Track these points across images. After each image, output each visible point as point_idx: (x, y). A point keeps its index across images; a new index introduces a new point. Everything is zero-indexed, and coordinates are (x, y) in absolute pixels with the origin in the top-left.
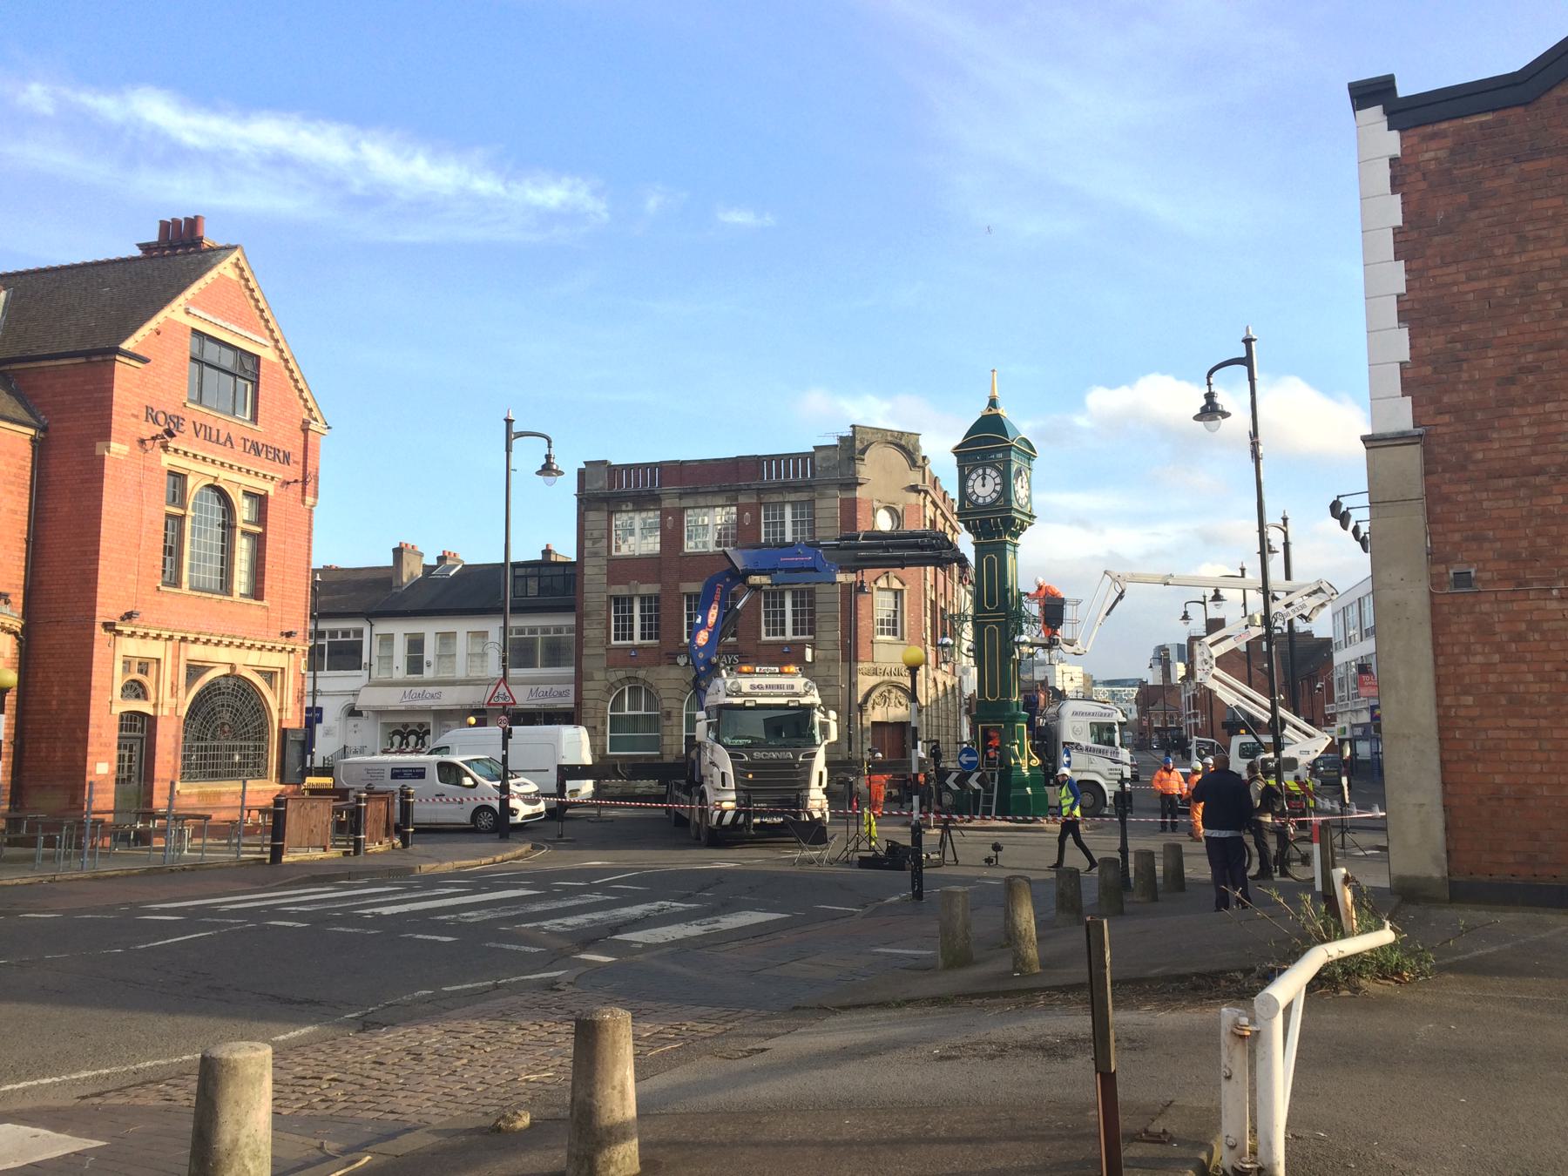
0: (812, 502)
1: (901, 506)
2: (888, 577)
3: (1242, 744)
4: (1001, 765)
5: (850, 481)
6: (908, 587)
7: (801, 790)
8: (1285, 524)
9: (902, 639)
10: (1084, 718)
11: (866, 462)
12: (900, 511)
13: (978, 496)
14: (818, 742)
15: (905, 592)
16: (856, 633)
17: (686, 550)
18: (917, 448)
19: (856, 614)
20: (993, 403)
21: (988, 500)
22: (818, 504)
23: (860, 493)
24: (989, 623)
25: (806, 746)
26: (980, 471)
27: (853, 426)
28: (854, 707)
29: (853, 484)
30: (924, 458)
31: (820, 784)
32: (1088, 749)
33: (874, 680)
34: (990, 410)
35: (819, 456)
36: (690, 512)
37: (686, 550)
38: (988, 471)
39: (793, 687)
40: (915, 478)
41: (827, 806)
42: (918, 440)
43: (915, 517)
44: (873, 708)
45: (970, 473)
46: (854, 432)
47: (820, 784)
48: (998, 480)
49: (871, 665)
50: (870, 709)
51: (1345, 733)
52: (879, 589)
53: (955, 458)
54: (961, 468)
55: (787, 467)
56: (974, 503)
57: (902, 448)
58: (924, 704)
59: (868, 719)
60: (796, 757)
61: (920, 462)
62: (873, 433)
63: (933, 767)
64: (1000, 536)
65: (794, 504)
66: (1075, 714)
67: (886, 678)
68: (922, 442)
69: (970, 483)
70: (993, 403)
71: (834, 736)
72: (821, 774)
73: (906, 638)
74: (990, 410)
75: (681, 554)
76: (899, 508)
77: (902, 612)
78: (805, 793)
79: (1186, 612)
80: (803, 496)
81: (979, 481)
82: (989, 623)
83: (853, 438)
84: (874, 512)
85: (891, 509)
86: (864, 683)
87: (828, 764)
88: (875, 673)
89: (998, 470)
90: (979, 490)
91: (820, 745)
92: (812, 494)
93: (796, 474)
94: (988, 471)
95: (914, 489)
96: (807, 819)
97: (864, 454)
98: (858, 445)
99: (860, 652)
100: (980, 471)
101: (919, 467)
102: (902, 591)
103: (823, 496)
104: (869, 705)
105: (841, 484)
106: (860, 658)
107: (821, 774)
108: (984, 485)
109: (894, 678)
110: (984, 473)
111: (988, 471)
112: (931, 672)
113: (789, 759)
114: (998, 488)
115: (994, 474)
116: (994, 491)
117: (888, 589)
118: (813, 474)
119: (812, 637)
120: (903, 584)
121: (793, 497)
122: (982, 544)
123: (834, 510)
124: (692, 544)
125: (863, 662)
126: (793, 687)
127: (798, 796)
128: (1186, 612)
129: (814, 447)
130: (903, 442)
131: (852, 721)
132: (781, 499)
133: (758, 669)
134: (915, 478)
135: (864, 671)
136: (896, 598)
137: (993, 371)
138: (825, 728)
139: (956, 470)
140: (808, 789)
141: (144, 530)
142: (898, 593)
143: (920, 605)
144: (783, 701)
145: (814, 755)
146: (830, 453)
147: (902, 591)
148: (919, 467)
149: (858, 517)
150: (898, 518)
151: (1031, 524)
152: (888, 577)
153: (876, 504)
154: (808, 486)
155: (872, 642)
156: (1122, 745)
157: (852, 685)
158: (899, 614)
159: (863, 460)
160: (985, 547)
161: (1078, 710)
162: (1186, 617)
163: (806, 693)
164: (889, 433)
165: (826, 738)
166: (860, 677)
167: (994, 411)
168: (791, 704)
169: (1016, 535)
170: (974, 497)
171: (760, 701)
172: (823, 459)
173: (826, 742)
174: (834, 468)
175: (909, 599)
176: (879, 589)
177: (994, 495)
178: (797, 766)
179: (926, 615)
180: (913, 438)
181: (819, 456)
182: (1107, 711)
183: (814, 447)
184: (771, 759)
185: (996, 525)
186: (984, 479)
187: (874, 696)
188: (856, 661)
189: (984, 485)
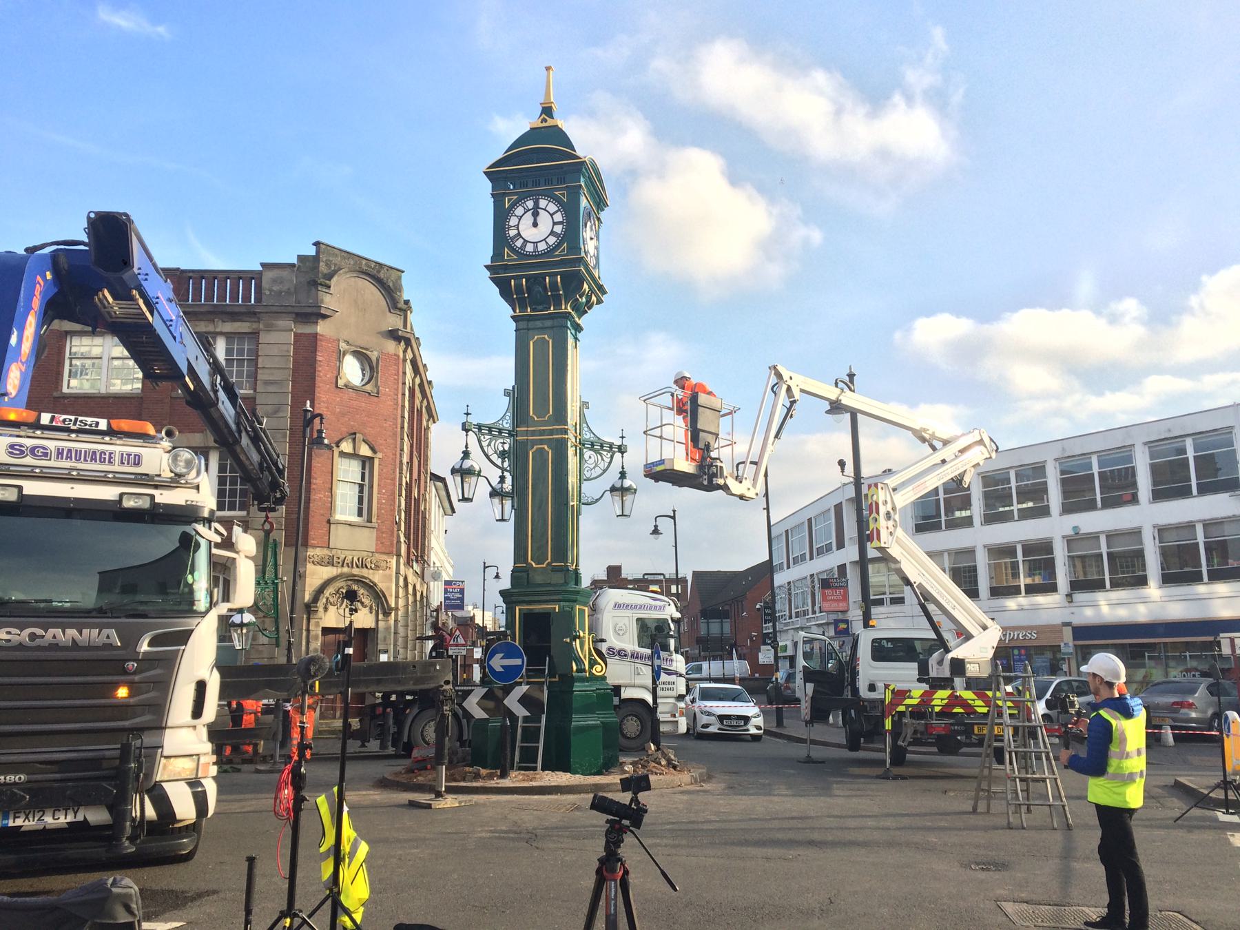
0: (254, 335)
1: (376, 353)
2: (354, 440)
3: (874, 641)
4: (551, 675)
5: (309, 310)
6: (379, 455)
7: (139, 731)
8: (852, 381)
9: (369, 521)
10: (628, 613)
11: (332, 290)
12: (374, 359)
13: (526, 241)
14: (202, 602)
15: (376, 462)
16: (307, 508)
17: (65, 390)
18: (399, 288)
19: (309, 483)
20: (547, 111)
21: (542, 247)
22: (264, 338)
23: (322, 328)
24: (534, 443)
25: (163, 614)
26: (530, 204)
27: (317, 244)
28: (299, 606)
29: (315, 315)
30: (407, 302)
31: (197, 712)
32: (634, 656)
33: (327, 572)
34: (544, 120)
35: (268, 276)
36: (76, 341)
37: (65, 390)
38: (543, 203)
39: (137, 460)
40: (394, 321)
41: (214, 770)
42: (400, 278)
43: (392, 370)
44: (326, 609)
45: (513, 206)
46: (318, 252)
47: (197, 712)
48: (558, 217)
49: (326, 552)
50: (321, 609)
51: (786, 651)
52: (343, 455)
53: (489, 184)
54: (498, 198)
55: (223, 289)
56: (520, 253)
57: (380, 283)
58: (393, 605)
59: (317, 624)
60: (130, 641)
61: (401, 305)
62: (344, 258)
63: (450, 677)
64: (558, 305)
65: (229, 337)
66: (618, 606)
67: (346, 570)
68: (405, 281)
69: (513, 221)
70: (547, 111)
71: (245, 590)
72: (201, 687)
73: (374, 520)
74: (544, 120)
75: (55, 394)
76: (374, 356)
77: (371, 487)
78: (148, 739)
79: (656, 526)
80: (243, 327)
81: (528, 219)
82: (534, 443)
83: (316, 258)
84: (340, 356)
85: (361, 355)
86: (316, 575)
87: (227, 666)
88: (331, 562)
89: (557, 200)
90: (528, 232)
91: (203, 614)
92: (255, 326)
93: (234, 297)
94: (543, 203)
95: (394, 335)
96: (150, 812)
97: (330, 279)
98: (323, 267)
99: (311, 533)
100: (530, 204)
101: (400, 309)
102: (371, 459)
103: (270, 328)
104: (321, 604)
105: (297, 314)
106: (312, 542)
107: (201, 687)
108: (535, 225)
109: (356, 571)
110: (536, 206)
111: (543, 203)
112: (402, 567)
113: (109, 647)
114: (558, 229)
115: (552, 208)
116: (552, 233)
117: (354, 456)
118: (258, 299)
119: (244, 513)
120: (374, 451)
121: (228, 327)
122: (529, 318)
123: (285, 347)
124: (74, 383)
125: (315, 547)
126: (137, 460)
127: (125, 750)
128: (656, 526)
129: (263, 265)
130: (382, 275)
131: (296, 624)
132: (211, 328)
133: (45, 418)
134: (394, 321)
135: (316, 559)
136: (363, 468)
137: (548, 69)
138: (222, 573)
139: (490, 203)
140: (160, 727)
141: (1042, 924)
142: (366, 462)
143: (394, 479)
144: (108, 493)
145: (184, 637)
146: (285, 273)
147: (371, 459)
148: (400, 309)
149: (319, 358)
150: (371, 368)
151: (599, 302)
152: (354, 440)
153: (343, 346)
154: (250, 314)
155: (329, 522)
156: (677, 652)
157: (298, 577)
158: (366, 489)
159: (329, 287)
160: (531, 324)
161: (621, 601)
162: (656, 531)
163: (176, 481)
164: (364, 262)
165: (226, 597)
166: (310, 567)
167: (550, 122)
168: (129, 503)
169: (582, 313)
170: (519, 243)
171: (33, 488)
172: (274, 281)
173: (223, 608)
174: (288, 292)
175: (381, 470)
176: (343, 455)
177: (552, 240)
178: (132, 665)
179: (400, 495)
180: (394, 274)
181: (268, 276)
182: (658, 603)
183: (263, 265)
184: (54, 647)
185: (554, 286)
186: (535, 214)
187: (327, 593)
188: (306, 545)
189: (535, 225)
